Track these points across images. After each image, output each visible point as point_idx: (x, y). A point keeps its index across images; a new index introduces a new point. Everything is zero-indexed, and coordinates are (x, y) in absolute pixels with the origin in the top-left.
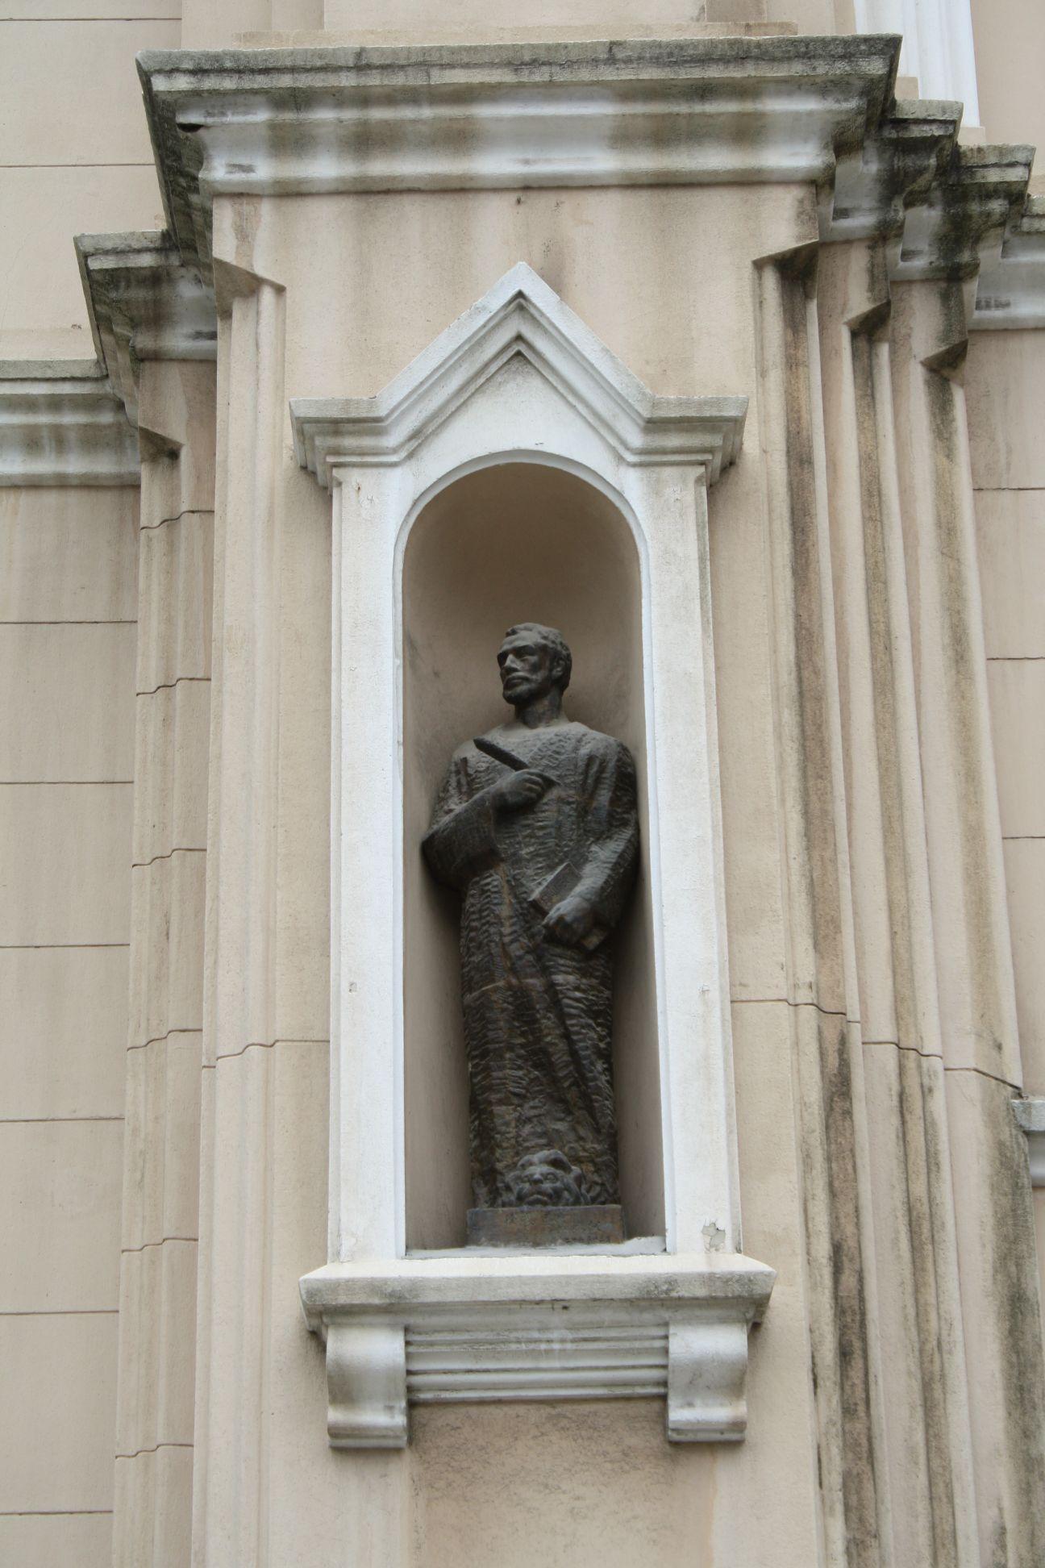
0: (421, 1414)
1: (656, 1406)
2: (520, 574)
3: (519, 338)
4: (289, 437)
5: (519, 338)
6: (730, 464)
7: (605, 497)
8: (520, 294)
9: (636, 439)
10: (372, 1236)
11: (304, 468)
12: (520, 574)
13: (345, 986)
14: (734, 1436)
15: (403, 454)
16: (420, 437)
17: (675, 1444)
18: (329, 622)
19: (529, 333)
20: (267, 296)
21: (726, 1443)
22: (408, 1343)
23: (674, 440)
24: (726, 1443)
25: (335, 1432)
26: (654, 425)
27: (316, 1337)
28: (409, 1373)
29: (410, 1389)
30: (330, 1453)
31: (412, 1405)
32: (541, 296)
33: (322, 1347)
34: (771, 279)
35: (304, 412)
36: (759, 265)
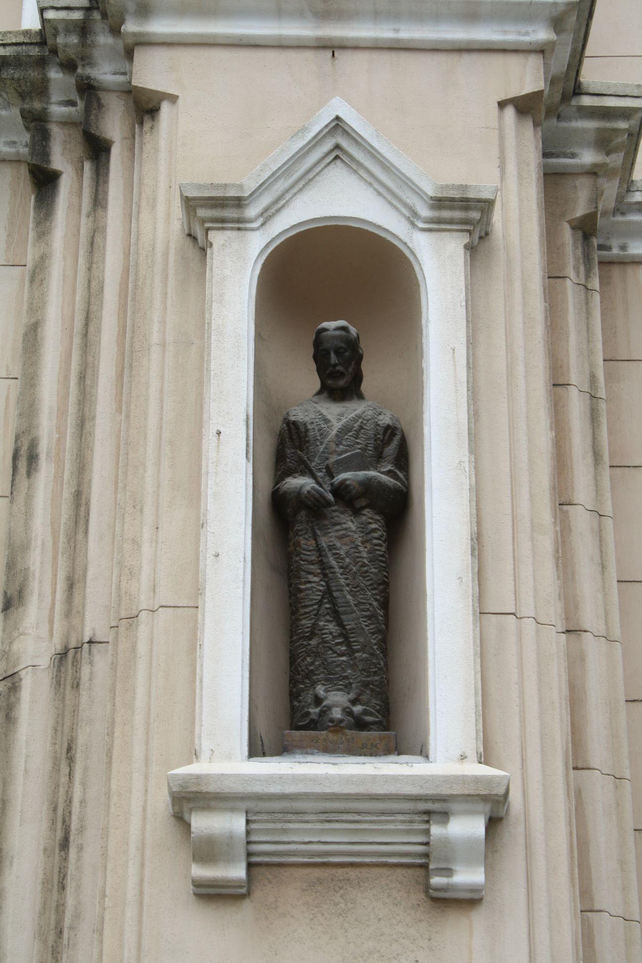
0: (256, 870)
1: (420, 872)
2: (335, 304)
3: (337, 147)
4: (178, 210)
5: (337, 147)
6: (485, 236)
7: (401, 252)
8: (338, 125)
9: (425, 212)
10: (223, 752)
11: (190, 235)
12: (335, 304)
13: (211, 552)
14: (476, 896)
15: (261, 220)
16: (268, 215)
17: (435, 900)
18: (194, 705)
19: (345, 143)
20: (165, 107)
21: (468, 902)
22: (248, 822)
23: (446, 214)
24: (468, 902)
25: (198, 884)
26: (439, 203)
27: (181, 820)
28: (248, 843)
29: (249, 854)
30: (192, 897)
31: (250, 866)
32: (352, 119)
33: (188, 825)
34: (510, 112)
35: (246, 753)
36: (502, 105)
